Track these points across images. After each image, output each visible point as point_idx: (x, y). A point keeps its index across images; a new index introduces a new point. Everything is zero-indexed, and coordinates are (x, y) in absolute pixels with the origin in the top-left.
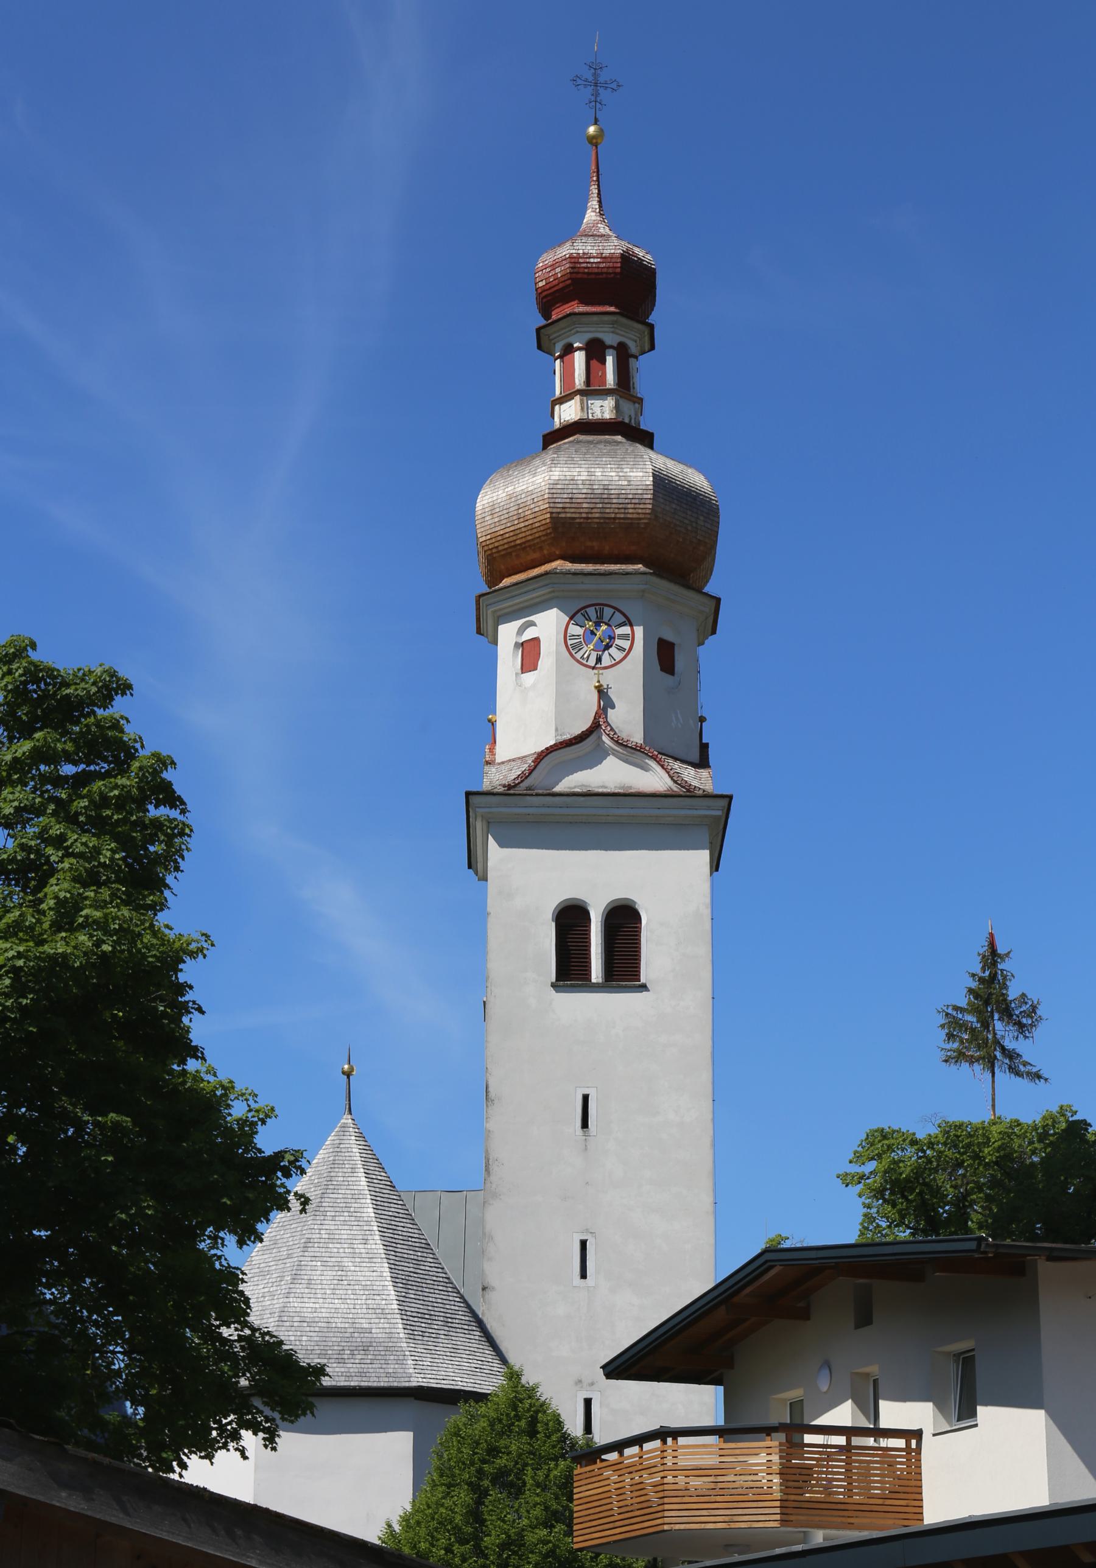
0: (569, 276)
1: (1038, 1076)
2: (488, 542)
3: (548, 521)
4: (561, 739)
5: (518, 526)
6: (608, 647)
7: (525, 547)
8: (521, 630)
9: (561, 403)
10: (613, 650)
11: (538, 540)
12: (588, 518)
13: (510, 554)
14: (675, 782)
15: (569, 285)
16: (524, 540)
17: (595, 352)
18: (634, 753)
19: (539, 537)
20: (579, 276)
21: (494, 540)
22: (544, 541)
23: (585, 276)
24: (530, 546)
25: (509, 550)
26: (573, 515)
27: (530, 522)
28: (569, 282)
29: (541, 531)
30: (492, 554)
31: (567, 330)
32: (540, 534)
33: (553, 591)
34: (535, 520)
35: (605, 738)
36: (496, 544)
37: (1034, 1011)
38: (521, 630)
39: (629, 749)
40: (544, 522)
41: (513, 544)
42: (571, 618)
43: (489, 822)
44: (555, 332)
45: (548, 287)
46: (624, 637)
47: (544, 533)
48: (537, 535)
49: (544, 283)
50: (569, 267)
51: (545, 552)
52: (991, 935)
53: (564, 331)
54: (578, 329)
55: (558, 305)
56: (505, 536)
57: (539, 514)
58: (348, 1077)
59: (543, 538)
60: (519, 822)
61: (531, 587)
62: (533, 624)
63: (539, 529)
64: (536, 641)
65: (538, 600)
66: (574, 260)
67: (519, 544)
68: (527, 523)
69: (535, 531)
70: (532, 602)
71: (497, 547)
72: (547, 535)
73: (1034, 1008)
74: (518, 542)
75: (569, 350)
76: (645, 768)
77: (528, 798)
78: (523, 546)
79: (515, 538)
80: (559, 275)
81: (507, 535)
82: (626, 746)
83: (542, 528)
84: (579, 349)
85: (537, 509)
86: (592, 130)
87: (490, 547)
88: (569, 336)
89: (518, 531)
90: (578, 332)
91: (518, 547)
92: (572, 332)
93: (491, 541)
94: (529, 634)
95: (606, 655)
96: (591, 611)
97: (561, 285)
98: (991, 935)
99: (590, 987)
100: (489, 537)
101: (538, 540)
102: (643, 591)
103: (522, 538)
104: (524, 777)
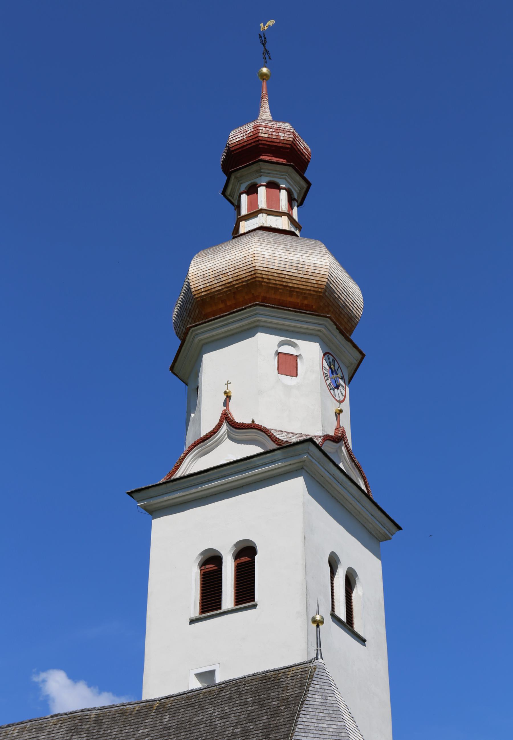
0: (291, 143)
2: (263, 272)
5: (296, 275)
7: (291, 291)
8: (281, 344)
9: (268, 214)
10: (339, 390)
11: (308, 292)
13: (279, 289)
15: (288, 148)
16: (296, 286)
18: (354, 468)
19: (310, 290)
20: (294, 147)
21: (269, 273)
22: (311, 294)
23: (297, 150)
24: (297, 292)
25: (278, 286)
26: (335, 290)
28: (290, 146)
29: (314, 287)
30: (262, 282)
31: (279, 173)
32: (312, 289)
33: (320, 331)
34: (312, 278)
35: (344, 449)
36: (270, 277)
38: (281, 344)
39: (353, 464)
40: (320, 283)
41: (284, 284)
43: (302, 468)
44: (268, 169)
45: (269, 140)
47: (316, 289)
48: (309, 288)
49: (266, 136)
50: (292, 138)
51: (306, 302)
53: (275, 172)
54: (287, 178)
55: (269, 155)
56: (280, 276)
57: (318, 275)
58: (318, 626)
59: (312, 292)
60: (314, 478)
61: (291, 317)
62: (294, 345)
63: (313, 285)
67: (289, 286)
68: (305, 276)
69: (309, 284)
70: (296, 329)
71: (270, 279)
72: (316, 292)
74: (291, 285)
78: (292, 289)
79: (289, 281)
80: (282, 138)
81: (283, 276)
83: (316, 286)
84: (283, 189)
85: (316, 271)
86: (265, 70)
87: (264, 276)
88: (276, 177)
89: (294, 278)
90: (285, 179)
91: (288, 288)
92: (282, 176)
93: (267, 273)
94: (286, 349)
97: (281, 145)
99: (350, 630)
100: (266, 269)
101: (308, 292)
102: (352, 364)
103: (295, 284)
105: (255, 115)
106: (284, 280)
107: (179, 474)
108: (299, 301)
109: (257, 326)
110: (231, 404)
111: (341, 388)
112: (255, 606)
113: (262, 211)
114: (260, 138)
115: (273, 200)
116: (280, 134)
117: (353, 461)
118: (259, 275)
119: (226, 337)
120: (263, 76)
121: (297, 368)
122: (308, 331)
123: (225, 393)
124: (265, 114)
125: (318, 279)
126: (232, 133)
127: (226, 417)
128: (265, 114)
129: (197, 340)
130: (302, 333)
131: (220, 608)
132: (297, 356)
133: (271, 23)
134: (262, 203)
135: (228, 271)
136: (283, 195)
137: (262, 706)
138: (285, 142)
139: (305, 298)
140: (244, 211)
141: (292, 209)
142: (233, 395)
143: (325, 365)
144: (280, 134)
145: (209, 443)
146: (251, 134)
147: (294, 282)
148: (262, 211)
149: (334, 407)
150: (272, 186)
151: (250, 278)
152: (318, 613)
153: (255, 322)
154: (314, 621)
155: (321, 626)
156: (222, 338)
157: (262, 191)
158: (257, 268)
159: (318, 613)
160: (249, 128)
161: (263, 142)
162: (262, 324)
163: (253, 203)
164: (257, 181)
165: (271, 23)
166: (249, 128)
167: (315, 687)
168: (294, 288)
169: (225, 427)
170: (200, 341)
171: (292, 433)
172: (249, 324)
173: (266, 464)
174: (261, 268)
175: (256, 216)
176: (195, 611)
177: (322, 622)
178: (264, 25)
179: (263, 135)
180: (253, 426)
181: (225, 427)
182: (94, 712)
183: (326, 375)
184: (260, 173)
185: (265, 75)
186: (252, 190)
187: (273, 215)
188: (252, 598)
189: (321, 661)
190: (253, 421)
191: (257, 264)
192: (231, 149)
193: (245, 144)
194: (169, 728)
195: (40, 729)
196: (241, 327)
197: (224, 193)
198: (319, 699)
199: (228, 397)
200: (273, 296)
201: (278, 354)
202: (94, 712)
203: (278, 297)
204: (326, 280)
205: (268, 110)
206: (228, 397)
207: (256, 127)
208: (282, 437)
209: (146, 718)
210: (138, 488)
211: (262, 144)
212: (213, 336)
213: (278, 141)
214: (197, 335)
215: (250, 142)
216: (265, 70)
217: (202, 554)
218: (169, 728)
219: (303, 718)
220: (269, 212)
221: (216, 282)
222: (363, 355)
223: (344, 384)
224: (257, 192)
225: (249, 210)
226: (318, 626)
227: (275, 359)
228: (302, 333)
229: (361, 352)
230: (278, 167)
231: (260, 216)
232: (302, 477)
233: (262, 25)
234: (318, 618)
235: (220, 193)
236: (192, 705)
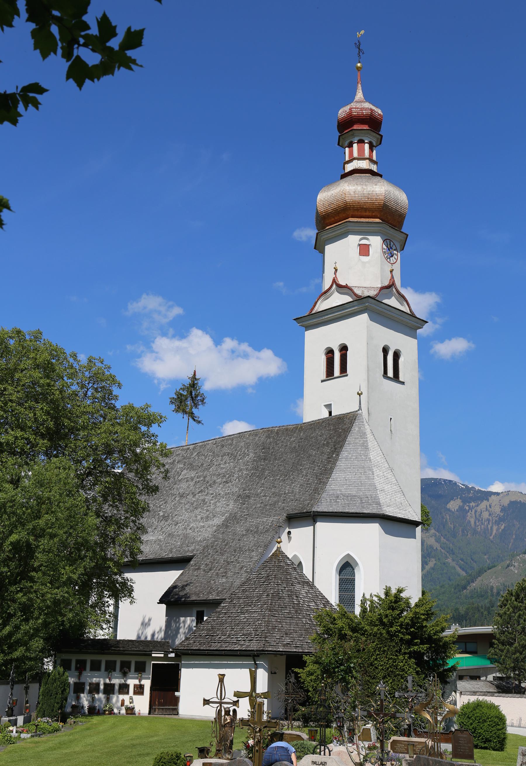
1: (199, 422)
3: (382, 204)
4: (384, 285)
6: (392, 256)
7: (366, 210)
9: (358, 160)
10: (393, 258)
12: (392, 207)
13: (359, 210)
14: (411, 312)
15: (368, 119)
16: (368, 207)
17: (372, 147)
24: (369, 210)
27: (374, 201)
28: (369, 118)
33: (381, 230)
35: (394, 290)
36: (354, 205)
37: (203, 400)
42: (383, 242)
45: (358, 116)
46: (396, 254)
48: (374, 207)
49: (356, 114)
52: (195, 371)
58: (360, 396)
59: (376, 209)
62: (367, 239)
64: (368, 246)
65: (333, 236)
66: (371, 110)
68: (372, 201)
73: (204, 399)
74: (365, 207)
75: (361, 142)
76: (402, 304)
77: (382, 304)
80: (365, 114)
82: (400, 294)
83: (378, 205)
84: (367, 143)
85: (378, 198)
86: (359, 65)
94: (364, 242)
95: (391, 258)
96: (388, 241)
97: (364, 117)
98: (195, 371)
100: (352, 201)
102: (401, 240)
104: (377, 295)
105: (351, 98)
106: (361, 205)
107: (314, 312)
108: (370, 214)
109: (348, 232)
110: (337, 274)
111: (395, 256)
112: (347, 375)
113: (355, 159)
114: (353, 116)
115: (361, 151)
116: (364, 111)
117: (400, 294)
118: (348, 204)
119: (335, 237)
120: (358, 69)
121: (369, 251)
122: (374, 231)
123: (334, 268)
124: (359, 95)
125: (379, 202)
126: (340, 112)
127: (334, 281)
128: (359, 95)
129: (322, 238)
130: (371, 232)
131: (333, 375)
132: (369, 245)
133: (362, 32)
134: (355, 154)
135: (334, 202)
136: (367, 146)
137: (336, 432)
138: (366, 115)
139: (373, 212)
140: (347, 159)
141: (372, 152)
142: (338, 268)
143: (384, 247)
144: (364, 111)
145: (328, 294)
146: (348, 113)
147: (367, 205)
148: (355, 159)
149: (388, 267)
150: (361, 142)
151: (344, 206)
152: (360, 390)
153: (347, 230)
154: (358, 394)
155: (361, 396)
156: (333, 238)
157: (355, 146)
158: (347, 201)
159: (360, 390)
160: (347, 109)
161: (355, 118)
162: (351, 230)
163: (351, 153)
164: (352, 140)
165: (362, 32)
166: (347, 109)
167: (357, 423)
168: (367, 208)
169: (334, 286)
170: (324, 239)
171: (365, 287)
172: (345, 230)
173: (351, 307)
174: (349, 201)
175: (352, 162)
176: (324, 377)
177: (362, 394)
178: (359, 33)
179: (354, 114)
180: (346, 287)
181: (334, 286)
182: (277, 429)
183: (384, 253)
184: (353, 136)
185: (360, 68)
186: (350, 146)
187: (361, 160)
188: (346, 372)
189: (360, 411)
190: (346, 284)
191: (347, 199)
192: (340, 122)
193: (346, 119)
194: (302, 439)
195: (256, 435)
196: (341, 232)
197: (339, 144)
198: (357, 429)
199: (336, 270)
200: (357, 213)
201: (360, 245)
202: (277, 429)
203: (360, 213)
204: (383, 202)
205: (361, 91)
206: (336, 270)
207: (350, 109)
208: (358, 292)
209: (295, 433)
210: (297, 317)
211: (354, 119)
212: (329, 237)
213: (363, 115)
214: (322, 236)
215: (348, 118)
216: (359, 65)
217: (326, 349)
218: (302, 439)
219: (349, 439)
220: (358, 159)
221: (329, 208)
222: (407, 235)
223: (396, 253)
224: (352, 146)
225: (349, 158)
226: (360, 396)
227: (357, 248)
228: (371, 232)
229: (406, 234)
230: (363, 131)
231: (354, 161)
232: (366, 314)
233: (358, 33)
234: (360, 392)
235: (336, 145)
236: (311, 429)
